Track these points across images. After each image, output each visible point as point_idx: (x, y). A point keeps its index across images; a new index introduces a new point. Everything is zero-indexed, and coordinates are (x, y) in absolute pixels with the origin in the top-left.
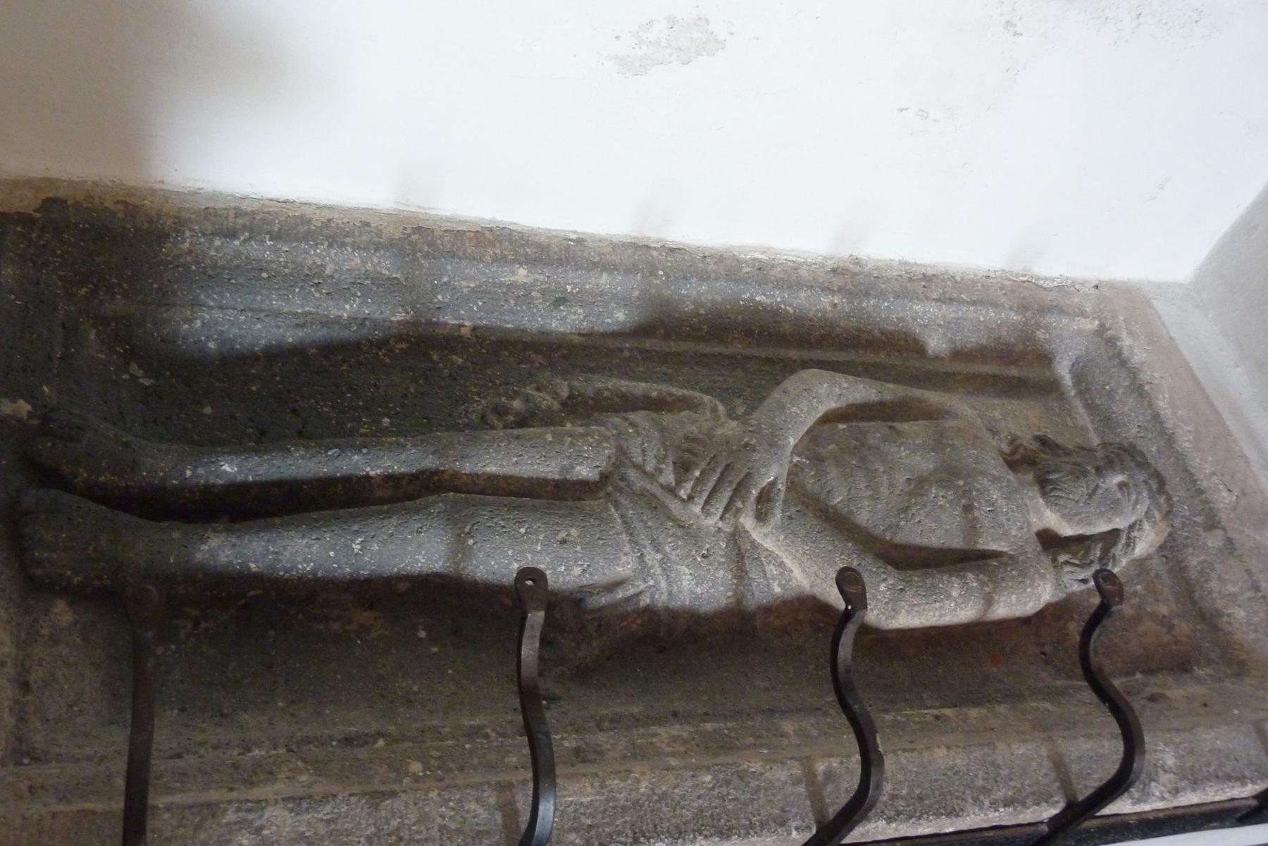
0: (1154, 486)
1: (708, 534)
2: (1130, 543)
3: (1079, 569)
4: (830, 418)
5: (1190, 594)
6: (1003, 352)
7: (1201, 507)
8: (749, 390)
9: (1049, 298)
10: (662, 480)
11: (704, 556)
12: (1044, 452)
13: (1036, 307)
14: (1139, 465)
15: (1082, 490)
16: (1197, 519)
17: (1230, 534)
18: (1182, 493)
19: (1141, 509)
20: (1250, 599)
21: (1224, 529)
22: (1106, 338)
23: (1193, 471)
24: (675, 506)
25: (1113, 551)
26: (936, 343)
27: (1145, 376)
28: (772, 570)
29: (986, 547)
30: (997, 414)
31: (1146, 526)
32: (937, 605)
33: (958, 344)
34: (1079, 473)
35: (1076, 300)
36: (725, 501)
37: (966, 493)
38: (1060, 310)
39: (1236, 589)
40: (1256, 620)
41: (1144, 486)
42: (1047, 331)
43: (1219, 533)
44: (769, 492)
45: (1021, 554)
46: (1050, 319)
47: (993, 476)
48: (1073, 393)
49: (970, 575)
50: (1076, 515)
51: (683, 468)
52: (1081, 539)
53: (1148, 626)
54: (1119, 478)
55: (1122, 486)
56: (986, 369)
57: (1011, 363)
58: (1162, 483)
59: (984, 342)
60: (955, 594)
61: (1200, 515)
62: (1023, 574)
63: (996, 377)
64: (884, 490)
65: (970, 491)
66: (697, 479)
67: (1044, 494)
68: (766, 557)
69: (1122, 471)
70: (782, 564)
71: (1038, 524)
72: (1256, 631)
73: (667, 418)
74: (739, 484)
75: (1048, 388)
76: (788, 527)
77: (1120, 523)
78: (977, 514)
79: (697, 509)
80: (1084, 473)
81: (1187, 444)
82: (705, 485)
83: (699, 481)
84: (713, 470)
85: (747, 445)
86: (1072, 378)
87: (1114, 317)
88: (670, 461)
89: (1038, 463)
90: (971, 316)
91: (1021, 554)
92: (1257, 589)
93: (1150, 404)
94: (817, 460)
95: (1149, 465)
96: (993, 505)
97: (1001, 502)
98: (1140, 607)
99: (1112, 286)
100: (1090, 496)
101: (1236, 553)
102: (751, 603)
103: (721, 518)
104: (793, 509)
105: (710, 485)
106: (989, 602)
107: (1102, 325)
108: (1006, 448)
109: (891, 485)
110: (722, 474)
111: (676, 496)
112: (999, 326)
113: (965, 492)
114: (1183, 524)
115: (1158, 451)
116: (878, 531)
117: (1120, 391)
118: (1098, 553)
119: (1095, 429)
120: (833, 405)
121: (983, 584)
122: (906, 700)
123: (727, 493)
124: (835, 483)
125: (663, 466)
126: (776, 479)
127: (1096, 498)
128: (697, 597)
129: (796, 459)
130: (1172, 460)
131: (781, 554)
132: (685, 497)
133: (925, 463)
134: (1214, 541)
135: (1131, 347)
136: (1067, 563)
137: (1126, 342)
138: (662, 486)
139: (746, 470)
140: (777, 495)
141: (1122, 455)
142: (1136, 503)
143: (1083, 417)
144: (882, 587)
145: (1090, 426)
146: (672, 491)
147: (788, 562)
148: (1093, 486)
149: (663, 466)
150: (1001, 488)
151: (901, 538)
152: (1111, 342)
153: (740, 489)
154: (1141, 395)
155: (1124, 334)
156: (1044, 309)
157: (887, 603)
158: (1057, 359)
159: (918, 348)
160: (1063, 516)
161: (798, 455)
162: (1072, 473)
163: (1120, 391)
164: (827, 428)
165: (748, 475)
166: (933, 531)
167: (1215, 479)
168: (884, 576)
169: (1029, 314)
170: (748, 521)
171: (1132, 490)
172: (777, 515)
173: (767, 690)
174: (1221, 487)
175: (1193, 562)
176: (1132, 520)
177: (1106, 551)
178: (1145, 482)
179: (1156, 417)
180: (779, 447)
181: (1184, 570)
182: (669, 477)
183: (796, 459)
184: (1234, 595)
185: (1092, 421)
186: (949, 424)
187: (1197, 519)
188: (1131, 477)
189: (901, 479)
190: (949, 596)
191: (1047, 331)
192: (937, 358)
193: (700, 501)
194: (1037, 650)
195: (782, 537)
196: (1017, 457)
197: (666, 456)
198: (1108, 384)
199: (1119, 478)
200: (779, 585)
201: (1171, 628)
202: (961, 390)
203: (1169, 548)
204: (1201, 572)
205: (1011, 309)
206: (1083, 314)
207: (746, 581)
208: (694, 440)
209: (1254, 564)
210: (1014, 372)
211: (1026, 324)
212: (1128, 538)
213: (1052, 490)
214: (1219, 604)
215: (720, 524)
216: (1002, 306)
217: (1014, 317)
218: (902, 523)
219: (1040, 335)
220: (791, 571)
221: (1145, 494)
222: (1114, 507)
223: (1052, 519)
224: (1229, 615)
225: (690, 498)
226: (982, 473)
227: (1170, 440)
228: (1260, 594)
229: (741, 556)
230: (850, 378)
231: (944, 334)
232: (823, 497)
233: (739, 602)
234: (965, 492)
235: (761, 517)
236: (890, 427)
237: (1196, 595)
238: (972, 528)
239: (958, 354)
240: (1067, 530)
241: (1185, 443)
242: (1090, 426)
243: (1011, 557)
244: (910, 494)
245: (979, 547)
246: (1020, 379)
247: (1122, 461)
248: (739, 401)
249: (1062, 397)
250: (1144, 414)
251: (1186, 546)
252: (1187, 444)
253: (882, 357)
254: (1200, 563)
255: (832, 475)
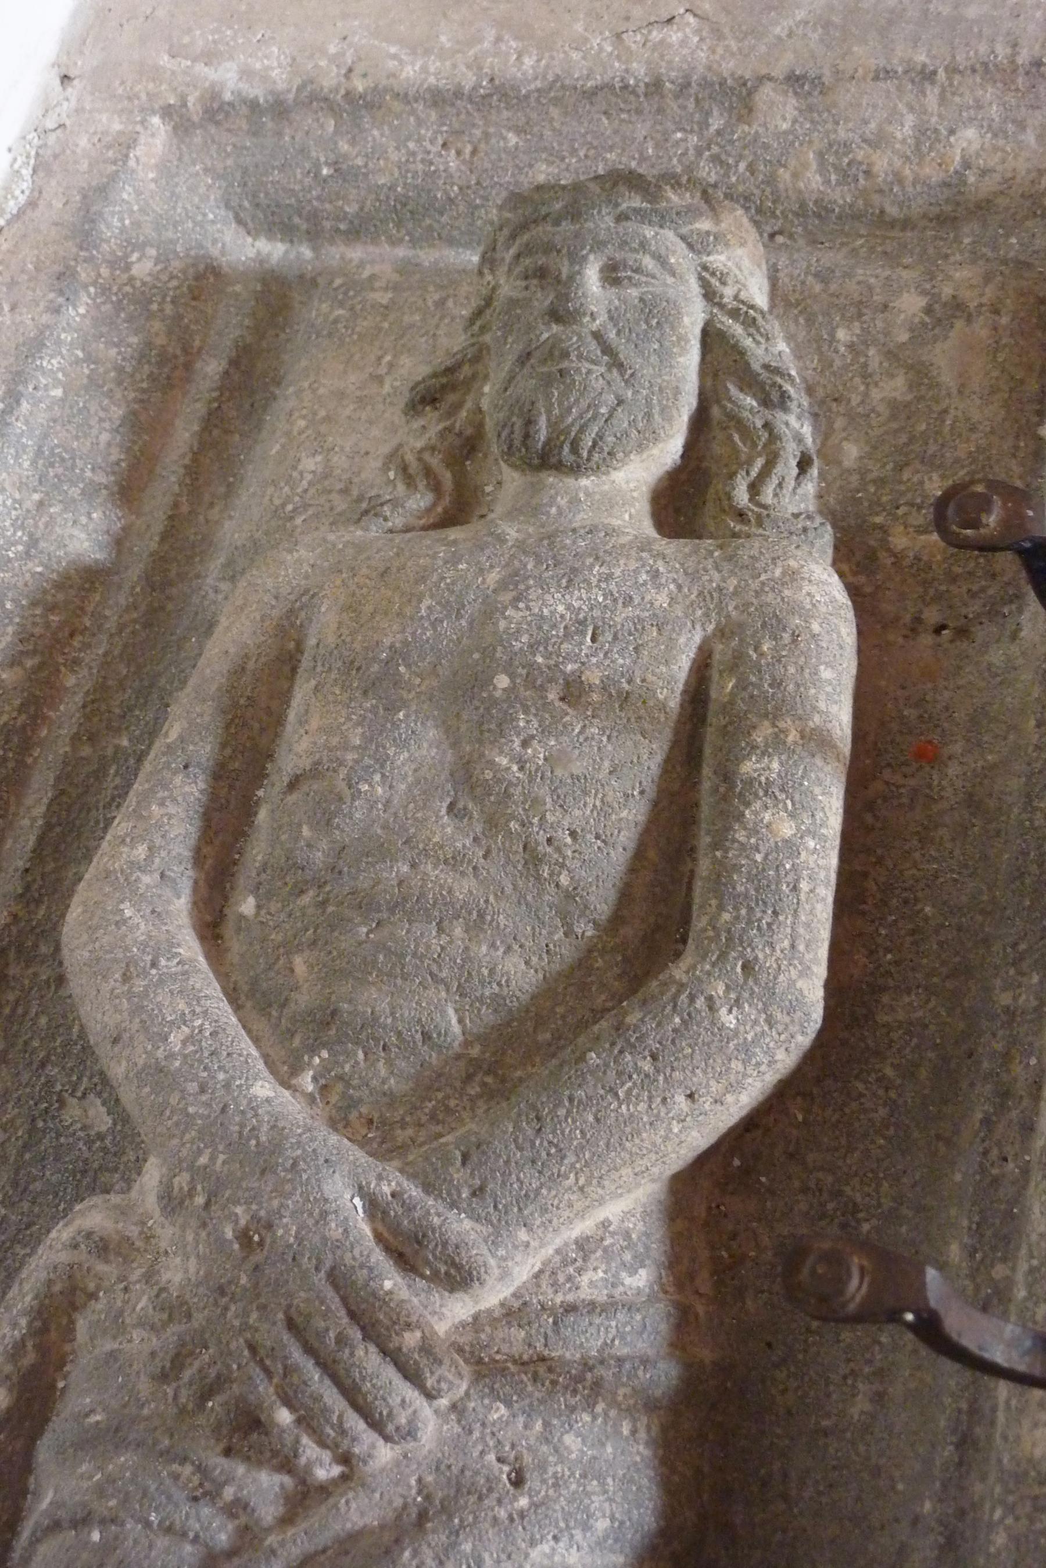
0: (636, 202)
1: (458, 1446)
2: (743, 312)
3: (779, 469)
4: (211, 925)
5: (882, 221)
6: (159, 375)
7: (691, 105)
8: (53, 1071)
9: (56, 204)
10: (268, 1512)
11: (518, 1482)
12: (458, 406)
13: (71, 247)
14: (574, 213)
15: (595, 374)
16: (716, 123)
17: (779, 71)
18: (641, 129)
19: (681, 257)
20: (942, 99)
21: (762, 79)
22: (203, 118)
23: (598, 79)
24: (358, 1512)
25: (756, 366)
26: (82, 535)
27: (330, 79)
28: (591, 1283)
29: (680, 686)
30: (310, 464)
31: (718, 260)
32: (804, 886)
33: (102, 478)
34: (549, 365)
35: (83, 142)
36: (390, 1373)
37: (534, 681)
38: (94, 197)
39: (910, 120)
40: (994, 111)
41: (631, 226)
42: (141, 247)
43: (767, 91)
44: (395, 1229)
45: (720, 608)
46: (112, 226)
47: (503, 585)
48: (307, 253)
49: (748, 767)
50: (648, 415)
51: (247, 1432)
52: (700, 423)
53: (943, 357)
54: (592, 275)
55: (612, 275)
56: (184, 434)
57: (188, 366)
58: (633, 181)
59: (118, 412)
60: (787, 829)
61: (708, 114)
62: (774, 624)
63: (214, 420)
64: (464, 888)
65: (531, 666)
66: (299, 1421)
67: (576, 470)
68: (555, 1285)
69: (577, 260)
70: (583, 1245)
71: (635, 518)
72: (1021, 126)
73: (82, 1401)
74: (352, 1315)
75: (276, 299)
76: (504, 1209)
77: (694, 317)
78: (593, 677)
79: (385, 1454)
80: (557, 352)
81: (528, 62)
82: (326, 1410)
83: (309, 1421)
84: (288, 1371)
85: (244, 1237)
86: (270, 235)
87: (156, 74)
88: (219, 1463)
89: (483, 440)
90: (42, 418)
91: (720, 608)
92: (928, 76)
93: (404, 97)
94: (324, 1025)
95: (577, 187)
96: (583, 623)
97: (578, 598)
98: (891, 355)
99: (76, 43)
100: (618, 365)
101: (827, 79)
102: (664, 1375)
103: (430, 1396)
104: (458, 1174)
105: (332, 1398)
106: (818, 741)
107: (167, 112)
108: (420, 501)
109: (455, 862)
110: (309, 1350)
111: (325, 1490)
112: (89, 359)
113: (530, 681)
114: (716, 159)
115: (519, 131)
116: (567, 952)
117: (344, 146)
118: (750, 401)
119: (414, 243)
120: (181, 905)
121: (778, 742)
122: (1006, 1057)
123: (368, 1359)
124: (407, 1012)
125: (229, 1493)
126: (361, 1191)
127: (625, 351)
128: (616, 1533)
129: (307, 1081)
130: (555, 112)
131: (558, 1242)
132: (337, 1470)
133: (420, 748)
134: (779, 113)
135: (246, 73)
136: (754, 489)
137: (228, 77)
138: (286, 1520)
139: (320, 1279)
140: (409, 1208)
141: (539, 232)
142: (661, 260)
143: (376, 258)
144: (729, 1019)
145: (401, 252)
146: (306, 1496)
147: (584, 1227)
148: (593, 345)
149: (229, 1493)
150: (543, 585)
151: (601, 902)
152: (216, 110)
153: (373, 1321)
154: (370, 106)
155: (210, 74)
156: (83, 229)
157: (770, 1022)
158: (215, 251)
159: (85, 582)
160: (641, 448)
161: (296, 1070)
162: (547, 381)
163: (344, 146)
164: (236, 946)
165: (333, 1277)
166: (605, 810)
167: (633, 40)
168: (700, 1003)
169: (84, 273)
170: (451, 1313)
171: (631, 258)
172: (461, 1226)
173: (879, 1398)
174: (656, 35)
175: (813, 181)
176: (695, 288)
177: (749, 381)
178: (622, 218)
179: (438, 99)
180: (276, 1147)
181: (823, 210)
182: (264, 1487)
183: (307, 1081)
184: (922, 131)
185: (394, 242)
186: (325, 626)
187: (716, 123)
188: (599, 245)
189: (443, 828)
190: (791, 847)
191: (141, 247)
192: (119, 543)
193: (365, 1438)
194: (927, 639)
195: (523, 1235)
196: (447, 478)
197: (201, 1469)
198: (317, 166)
199: (592, 275)
200: (633, 1272)
201: (957, 307)
202: (214, 513)
203: (783, 220)
204: (845, 177)
205: (57, 311)
206: (126, 144)
207: (607, 1374)
208: (178, 1361)
209: (865, 55)
210: (212, 368)
211: (105, 290)
212: (734, 314)
213: (575, 449)
214: (932, 173)
215: (444, 1402)
216: (43, 330)
217: (79, 311)
218: (564, 880)
219: (143, 268)
220: (605, 1224)
221: (649, 232)
222: (656, 314)
223: (636, 476)
224: (967, 165)
225: (345, 1459)
226: (490, 612)
227: (501, 95)
228: (941, 75)
229: (538, 1367)
230: (121, 826)
231: (68, 504)
232: (434, 1059)
233: (651, 1406)
234: (530, 681)
235: (458, 1277)
236: (293, 785)
237: (892, 211)
238: (625, 701)
239: (127, 491)
240: (670, 449)
241: (526, 67)
242: (401, 252)
243: (721, 633)
244: (493, 823)
245: (674, 703)
246: (234, 363)
247: (549, 248)
248: (72, 1112)
249: (308, 282)
250: (420, 123)
251: (771, 180)
252: (528, 62)
253: (77, 685)
254: (822, 167)
255: (384, 1006)
